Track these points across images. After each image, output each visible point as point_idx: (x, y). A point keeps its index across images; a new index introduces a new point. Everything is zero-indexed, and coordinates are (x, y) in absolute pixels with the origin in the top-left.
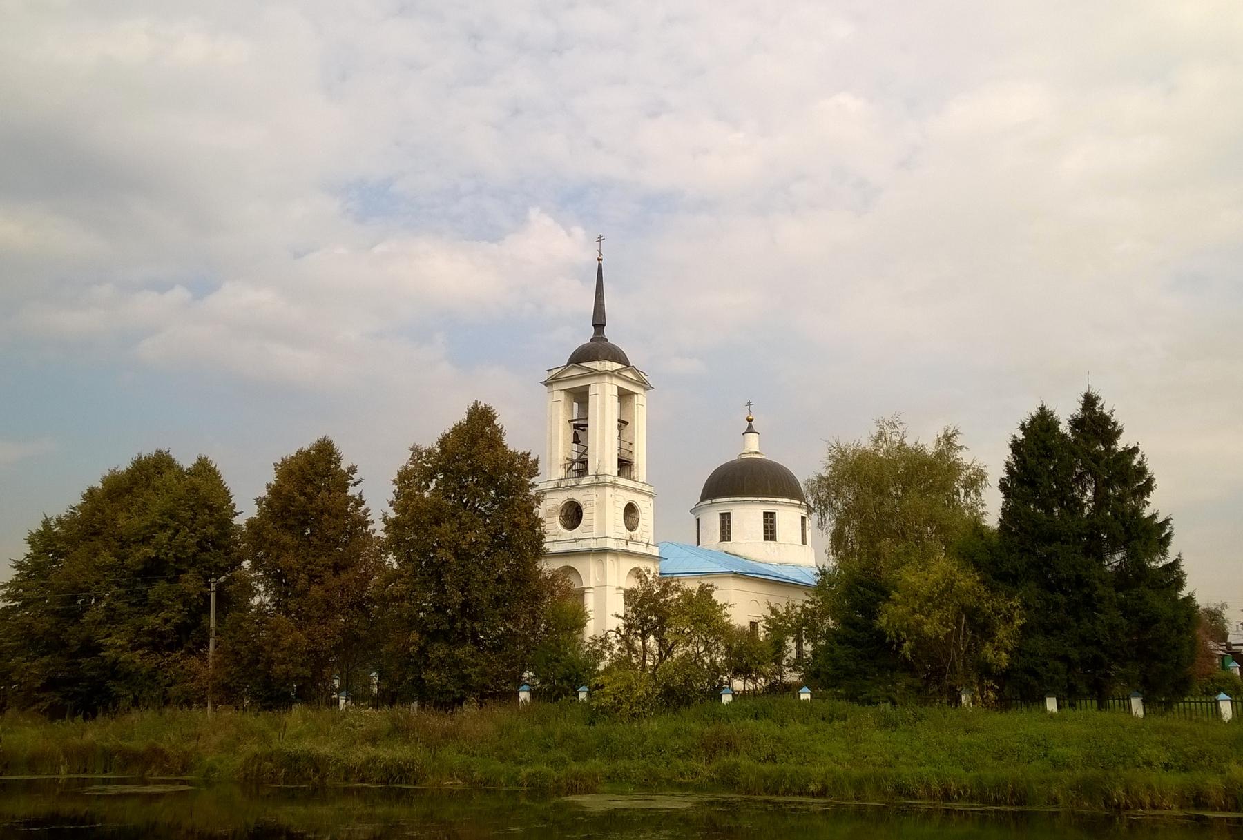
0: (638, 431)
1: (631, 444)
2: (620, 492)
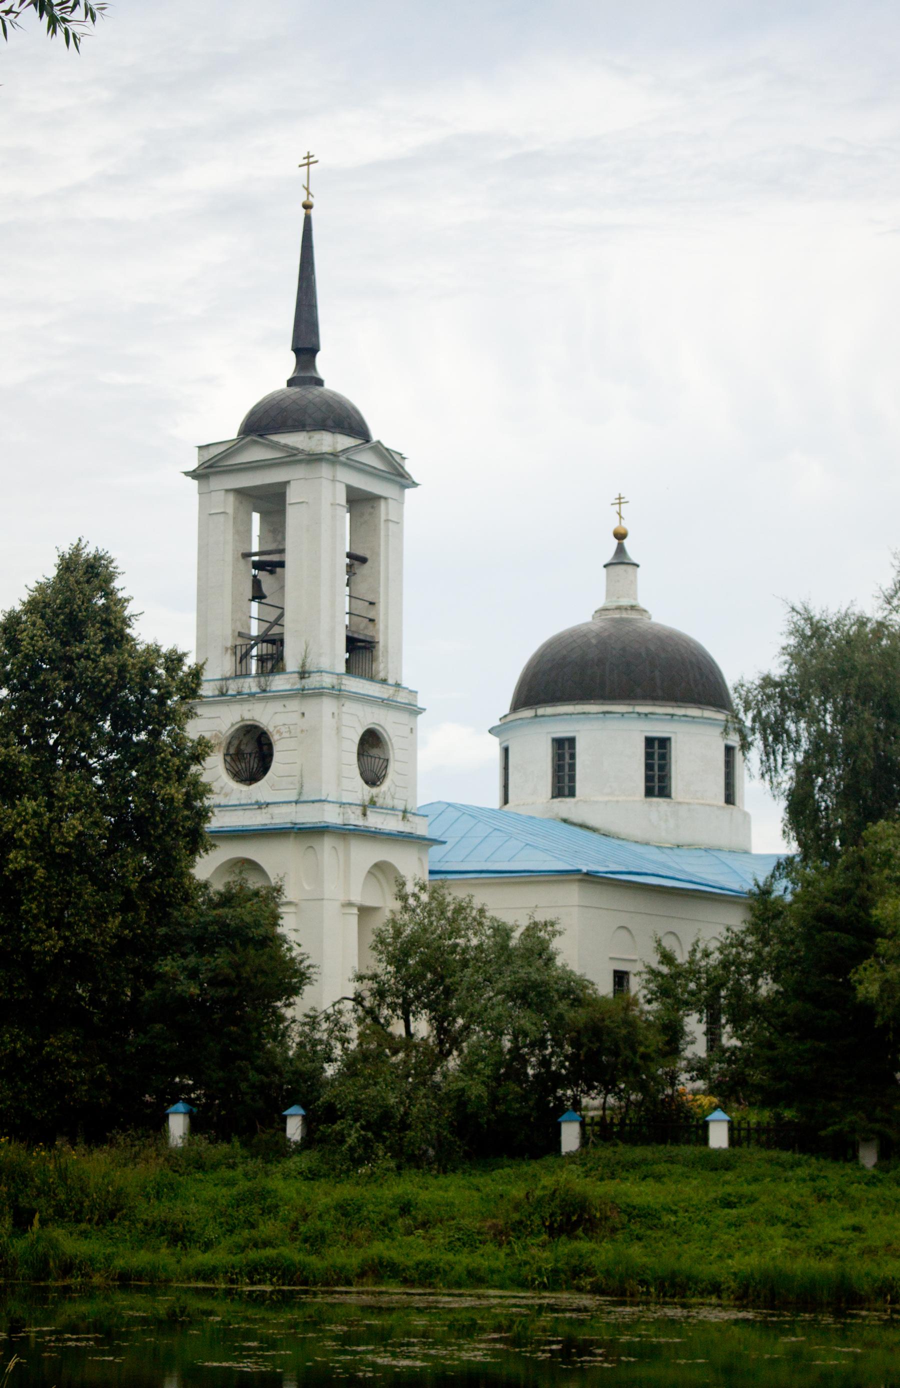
0: (387, 578)
1: (372, 603)
2: (350, 707)
